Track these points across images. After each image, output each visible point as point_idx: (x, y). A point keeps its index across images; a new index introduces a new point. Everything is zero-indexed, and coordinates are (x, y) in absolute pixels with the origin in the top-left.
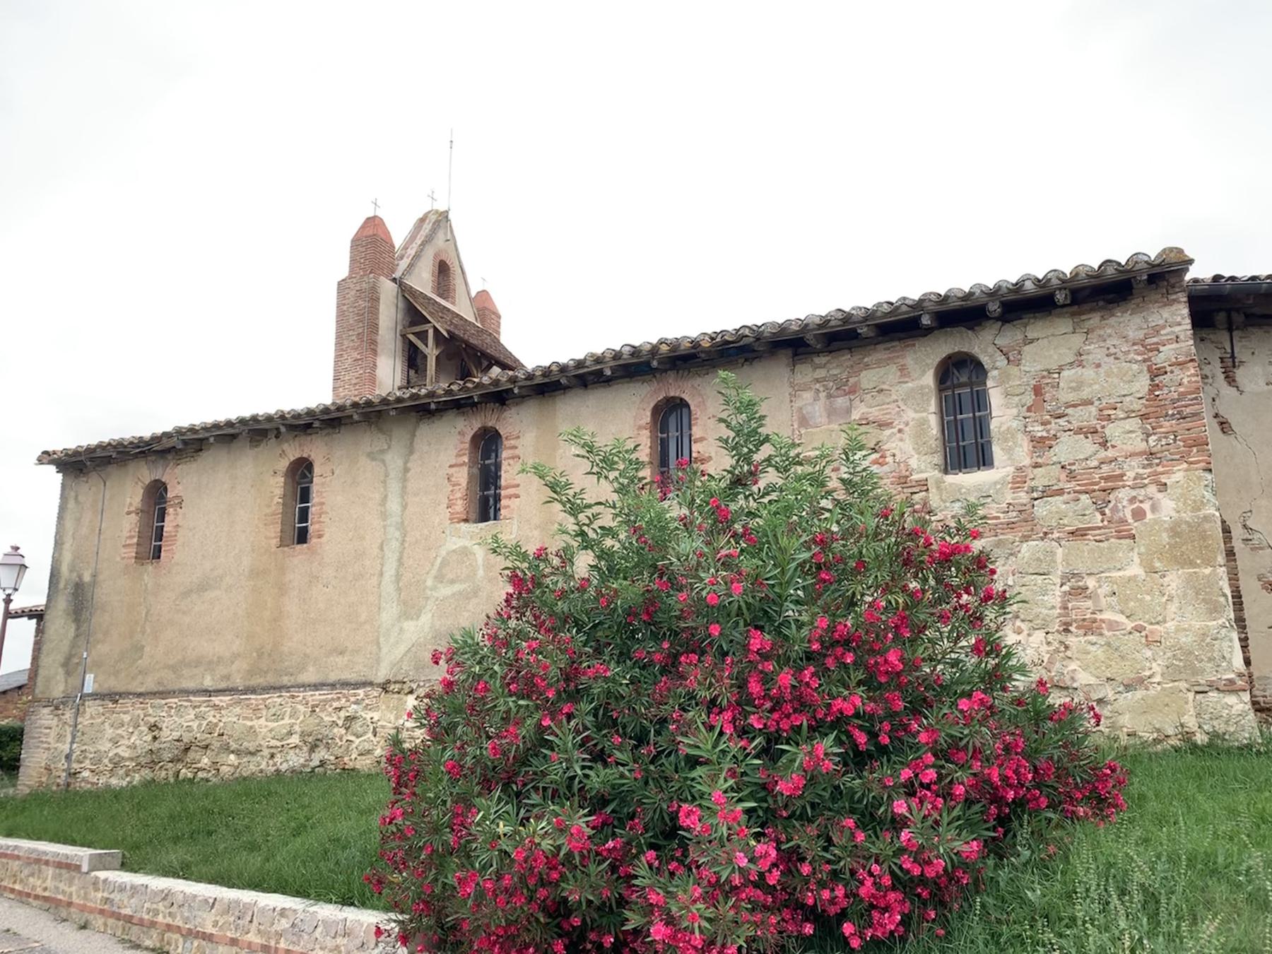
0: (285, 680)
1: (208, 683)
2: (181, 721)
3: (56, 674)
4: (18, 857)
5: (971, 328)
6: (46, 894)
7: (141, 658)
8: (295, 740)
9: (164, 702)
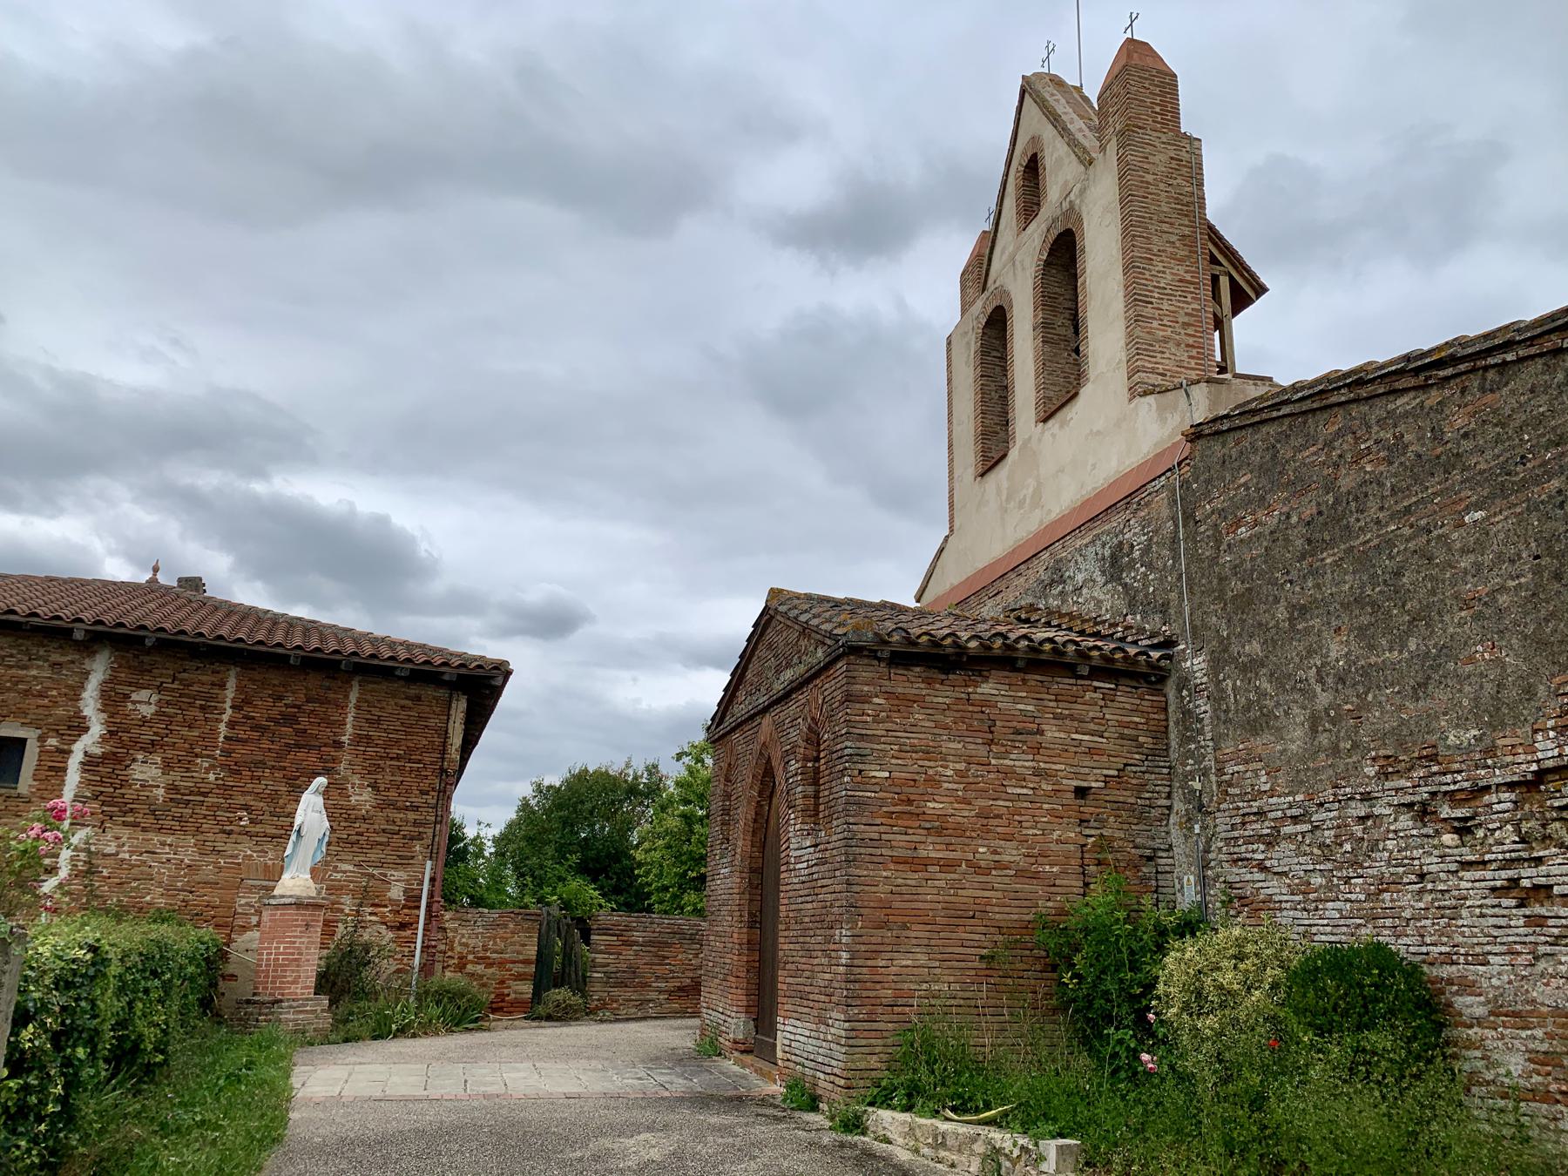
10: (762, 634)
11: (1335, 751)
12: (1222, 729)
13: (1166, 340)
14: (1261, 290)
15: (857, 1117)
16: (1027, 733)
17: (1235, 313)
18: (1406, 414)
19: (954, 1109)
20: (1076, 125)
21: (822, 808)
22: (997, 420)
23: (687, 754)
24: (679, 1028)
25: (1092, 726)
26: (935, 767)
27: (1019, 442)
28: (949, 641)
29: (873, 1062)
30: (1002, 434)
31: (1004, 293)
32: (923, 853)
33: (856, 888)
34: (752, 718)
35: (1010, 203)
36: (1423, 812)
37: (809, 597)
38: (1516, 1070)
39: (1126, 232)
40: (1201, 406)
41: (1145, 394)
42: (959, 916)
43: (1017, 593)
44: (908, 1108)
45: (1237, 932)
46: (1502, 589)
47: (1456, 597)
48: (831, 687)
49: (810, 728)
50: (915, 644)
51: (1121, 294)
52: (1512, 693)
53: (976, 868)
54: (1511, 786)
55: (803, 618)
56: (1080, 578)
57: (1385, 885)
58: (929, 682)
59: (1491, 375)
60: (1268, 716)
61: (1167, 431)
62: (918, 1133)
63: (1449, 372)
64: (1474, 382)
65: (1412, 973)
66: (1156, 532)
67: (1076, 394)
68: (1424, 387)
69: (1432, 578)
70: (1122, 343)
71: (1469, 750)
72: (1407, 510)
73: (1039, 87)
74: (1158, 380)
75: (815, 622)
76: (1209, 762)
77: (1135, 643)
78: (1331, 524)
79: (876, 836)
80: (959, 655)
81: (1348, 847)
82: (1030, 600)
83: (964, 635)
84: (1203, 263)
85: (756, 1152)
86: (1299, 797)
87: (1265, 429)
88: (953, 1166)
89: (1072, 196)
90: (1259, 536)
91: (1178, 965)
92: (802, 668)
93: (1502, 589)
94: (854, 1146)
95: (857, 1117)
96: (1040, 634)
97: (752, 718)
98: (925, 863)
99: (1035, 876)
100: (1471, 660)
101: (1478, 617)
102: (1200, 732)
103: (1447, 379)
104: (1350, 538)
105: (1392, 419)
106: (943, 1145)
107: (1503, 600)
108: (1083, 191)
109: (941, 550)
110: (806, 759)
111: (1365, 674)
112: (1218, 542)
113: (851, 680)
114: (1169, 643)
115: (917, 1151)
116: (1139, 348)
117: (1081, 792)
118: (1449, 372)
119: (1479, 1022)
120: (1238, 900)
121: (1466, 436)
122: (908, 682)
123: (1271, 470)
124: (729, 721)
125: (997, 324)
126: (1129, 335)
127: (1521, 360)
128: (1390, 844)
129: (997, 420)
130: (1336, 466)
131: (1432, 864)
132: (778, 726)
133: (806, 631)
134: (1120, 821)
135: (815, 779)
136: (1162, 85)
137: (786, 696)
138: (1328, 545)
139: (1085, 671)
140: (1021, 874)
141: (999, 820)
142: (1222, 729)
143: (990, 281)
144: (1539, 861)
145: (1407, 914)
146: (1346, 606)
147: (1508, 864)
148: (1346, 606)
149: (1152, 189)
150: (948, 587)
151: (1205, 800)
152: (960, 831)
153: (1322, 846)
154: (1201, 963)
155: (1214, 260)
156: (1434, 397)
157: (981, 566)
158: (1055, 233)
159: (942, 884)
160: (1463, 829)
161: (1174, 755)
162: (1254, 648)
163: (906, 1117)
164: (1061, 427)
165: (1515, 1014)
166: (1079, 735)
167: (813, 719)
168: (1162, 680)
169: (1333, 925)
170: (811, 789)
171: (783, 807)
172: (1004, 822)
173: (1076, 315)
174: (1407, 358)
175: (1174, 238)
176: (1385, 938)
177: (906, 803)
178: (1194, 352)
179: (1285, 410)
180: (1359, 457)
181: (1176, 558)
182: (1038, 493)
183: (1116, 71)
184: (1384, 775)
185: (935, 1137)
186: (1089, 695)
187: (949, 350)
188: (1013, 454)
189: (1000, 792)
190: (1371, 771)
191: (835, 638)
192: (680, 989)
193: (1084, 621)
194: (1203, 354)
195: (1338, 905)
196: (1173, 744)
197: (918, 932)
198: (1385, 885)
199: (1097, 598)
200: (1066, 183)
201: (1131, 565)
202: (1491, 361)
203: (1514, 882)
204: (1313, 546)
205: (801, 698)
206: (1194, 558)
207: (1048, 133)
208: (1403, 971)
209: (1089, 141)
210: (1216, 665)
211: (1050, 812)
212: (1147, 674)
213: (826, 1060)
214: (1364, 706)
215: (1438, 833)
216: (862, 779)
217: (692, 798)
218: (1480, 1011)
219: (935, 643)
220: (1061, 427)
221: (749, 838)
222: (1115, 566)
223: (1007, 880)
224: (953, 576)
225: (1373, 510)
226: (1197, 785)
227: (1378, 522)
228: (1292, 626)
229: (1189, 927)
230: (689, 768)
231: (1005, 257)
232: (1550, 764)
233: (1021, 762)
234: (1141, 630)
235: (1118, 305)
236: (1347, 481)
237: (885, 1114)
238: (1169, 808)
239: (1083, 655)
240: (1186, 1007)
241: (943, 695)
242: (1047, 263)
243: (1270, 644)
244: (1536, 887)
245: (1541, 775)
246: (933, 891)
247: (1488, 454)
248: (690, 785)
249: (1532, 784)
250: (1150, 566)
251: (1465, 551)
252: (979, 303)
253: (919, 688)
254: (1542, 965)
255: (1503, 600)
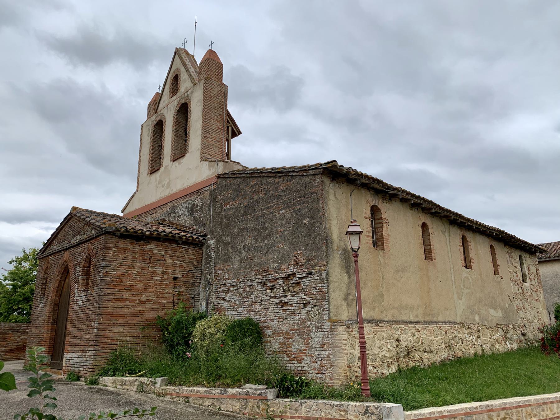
0: (435, 319)
1: (412, 318)
2: (408, 338)
3: (342, 305)
4: (530, 405)
5: (505, 246)
6: (556, 415)
7: (383, 301)
8: (443, 346)
9: (398, 326)
10: (67, 222)
11: (245, 268)
12: (217, 261)
13: (212, 145)
14: (240, 133)
15: (96, 380)
16: (161, 261)
17: (233, 137)
18: (271, 183)
19: (129, 374)
20: (192, 70)
21: (90, 283)
22: (157, 156)
23: (14, 261)
24: (19, 363)
25: (181, 259)
26: (131, 271)
27: (164, 166)
28: (140, 231)
29: (102, 363)
30: (158, 161)
31: (163, 116)
32: (124, 297)
33: (101, 309)
34: (60, 251)
35: (167, 87)
36: (264, 284)
37: (87, 211)
38: (276, 347)
39: (204, 110)
40: (220, 169)
41: (205, 161)
42: (134, 316)
43: (159, 214)
44: (113, 375)
45: (216, 317)
46: (286, 230)
47: (276, 231)
48: (98, 244)
49: (87, 257)
50: (129, 232)
51: (201, 129)
52: (285, 255)
53: (141, 302)
54: (283, 278)
55: (88, 219)
56: (180, 213)
57: (254, 303)
58: (131, 244)
59: (289, 178)
60: (230, 258)
61: (211, 173)
62: (117, 382)
63: (281, 175)
64: (286, 178)
65: (257, 325)
66: (205, 202)
67: (184, 155)
68: (275, 177)
69: (272, 226)
70: (200, 143)
71: (275, 269)
72: (268, 208)
73: (181, 53)
74: (209, 157)
75: (93, 221)
76: (213, 270)
77: (195, 234)
78: (250, 208)
79: (110, 292)
80: (143, 236)
81: (246, 293)
82: (163, 217)
83: (145, 230)
84: (225, 124)
85: (62, 393)
86: (235, 280)
87: (237, 179)
88: (128, 390)
89: (188, 93)
90: (232, 208)
91: (200, 325)
92: (85, 236)
93: (286, 230)
94: (95, 388)
95: (96, 380)
96: (168, 230)
97: (60, 251)
98: (125, 300)
99: (159, 303)
100: (278, 247)
101: (281, 236)
102: (211, 261)
103: (280, 176)
104: (255, 212)
105: (267, 183)
106: (125, 384)
107: (286, 233)
108: (192, 93)
109: (133, 196)
110: (84, 267)
111: (254, 248)
112: (222, 208)
113: (106, 242)
114: (205, 235)
115: (116, 387)
116: (205, 147)
117: (175, 278)
118: (281, 175)
119: (270, 336)
120: (217, 309)
121: (283, 191)
122: (125, 244)
123: (237, 190)
124: (48, 252)
125: (160, 126)
126: (202, 142)
127: (296, 176)
128: (256, 292)
129: (157, 156)
130: (254, 193)
131: (264, 298)
132: (73, 255)
133: (88, 224)
134: (186, 288)
135: (88, 273)
136: (219, 67)
137: (77, 245)
138: (250, 213)
139: (181, 243)
140: (155, 303)
141: (147, 286)
142: (217, 261)
143: (158, 111)
144: (286, 296)
145: (257, 310)
146: (252, 230)
147: (280, 297)
148: (252, 230)
149: (213, 98)
150: (134, 209)
151: (210, 281)
152: (137, 290)
153: (240, 293)
154: (206, 326)
155: (228, 122)
156: (277, 180)
157: (147, 203)
158: (181, 103)
159: (130, 307)
160: (272, 289)
161: (203, 268)
162: (228, 239)
163: (114, 378)
164: (179, 164)
165: (278, 334)
166: (176, 261)
167: (89, 254)
168: (202, 246)
169: (240, 314)
170: (85, 277)
171: (73, 282)
172: (151, 287)
173: (186, 129)
174: (272, 169)
175: (217, 115)
176: (252, 317)
177: (121, 282)
178: (220, 150)
179: (243, 175)
180: (259, 192)
181: (210, 211)
182: (169, 184)
183: (206, 58)
184: (256, 275)
185: (123, 382)
186: (181, 249)
187: (142, 129)
188: (162, 169)
189: (151, 278)
190: (253, 274)
191: (101, 228)
192: (11, 350)
193: (180, 226)
194: (222, 149)
195: (242, 309)
196: (203, 264)
197: (120, 321)
198: (254, 303)
199: (186, 219)
200: (187, 87)
201: (197, 211)
202: (290, 174)
203: (281, 301)
204: (246, 213)
205: (84, 246)
206: (215, 212)
207: (183, 69)
208: (255, 325)
209: (195, 76)
210: (217, 243)
211: (166, 285)
212: (198, 244)
213: (85, 364)
214: (254, 257)
215: (266, 289)
216: (107, 274)
217: (17, 278)
218: (270, 334)
219: (135, 232)
220: (179, 164)
221: (55, 293)
222: (192, 210)
223: (150, 305)
224: (136, 206)
225: (261, 207)
226: (209, 276)
227: (262, 209)
228: (239, 234)
229: (202, 317)
230: (16, 267)
231: (164, 104)
232: (291, 273)
233: (158, 269)
234: (198, 231)
235: (200, 132)
236: (255, 198)
237: (106, 378)
238: (200, 283)
239: (180, 238)
240: (200, 338)
241: (136, 248)
242: (179, 111)
243: (233, 238)
244: (285, 302)
245: (289, 275)
246: (127, 309)
247: (287, 197)
248: (17, 274)
249: (287, 278)
250: (202, 212)
251: (280, 220)
252: (154, 117)
253: (128, 246)
254: (284, 321)
255: (286, 233)
